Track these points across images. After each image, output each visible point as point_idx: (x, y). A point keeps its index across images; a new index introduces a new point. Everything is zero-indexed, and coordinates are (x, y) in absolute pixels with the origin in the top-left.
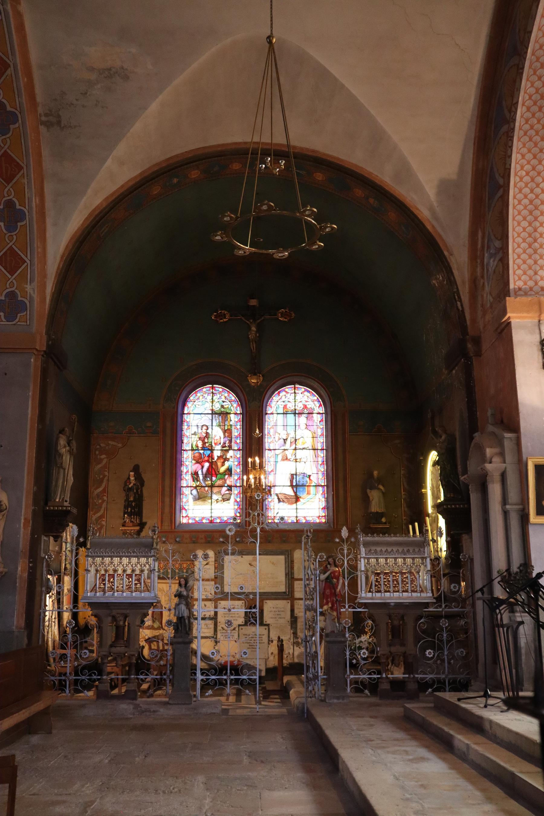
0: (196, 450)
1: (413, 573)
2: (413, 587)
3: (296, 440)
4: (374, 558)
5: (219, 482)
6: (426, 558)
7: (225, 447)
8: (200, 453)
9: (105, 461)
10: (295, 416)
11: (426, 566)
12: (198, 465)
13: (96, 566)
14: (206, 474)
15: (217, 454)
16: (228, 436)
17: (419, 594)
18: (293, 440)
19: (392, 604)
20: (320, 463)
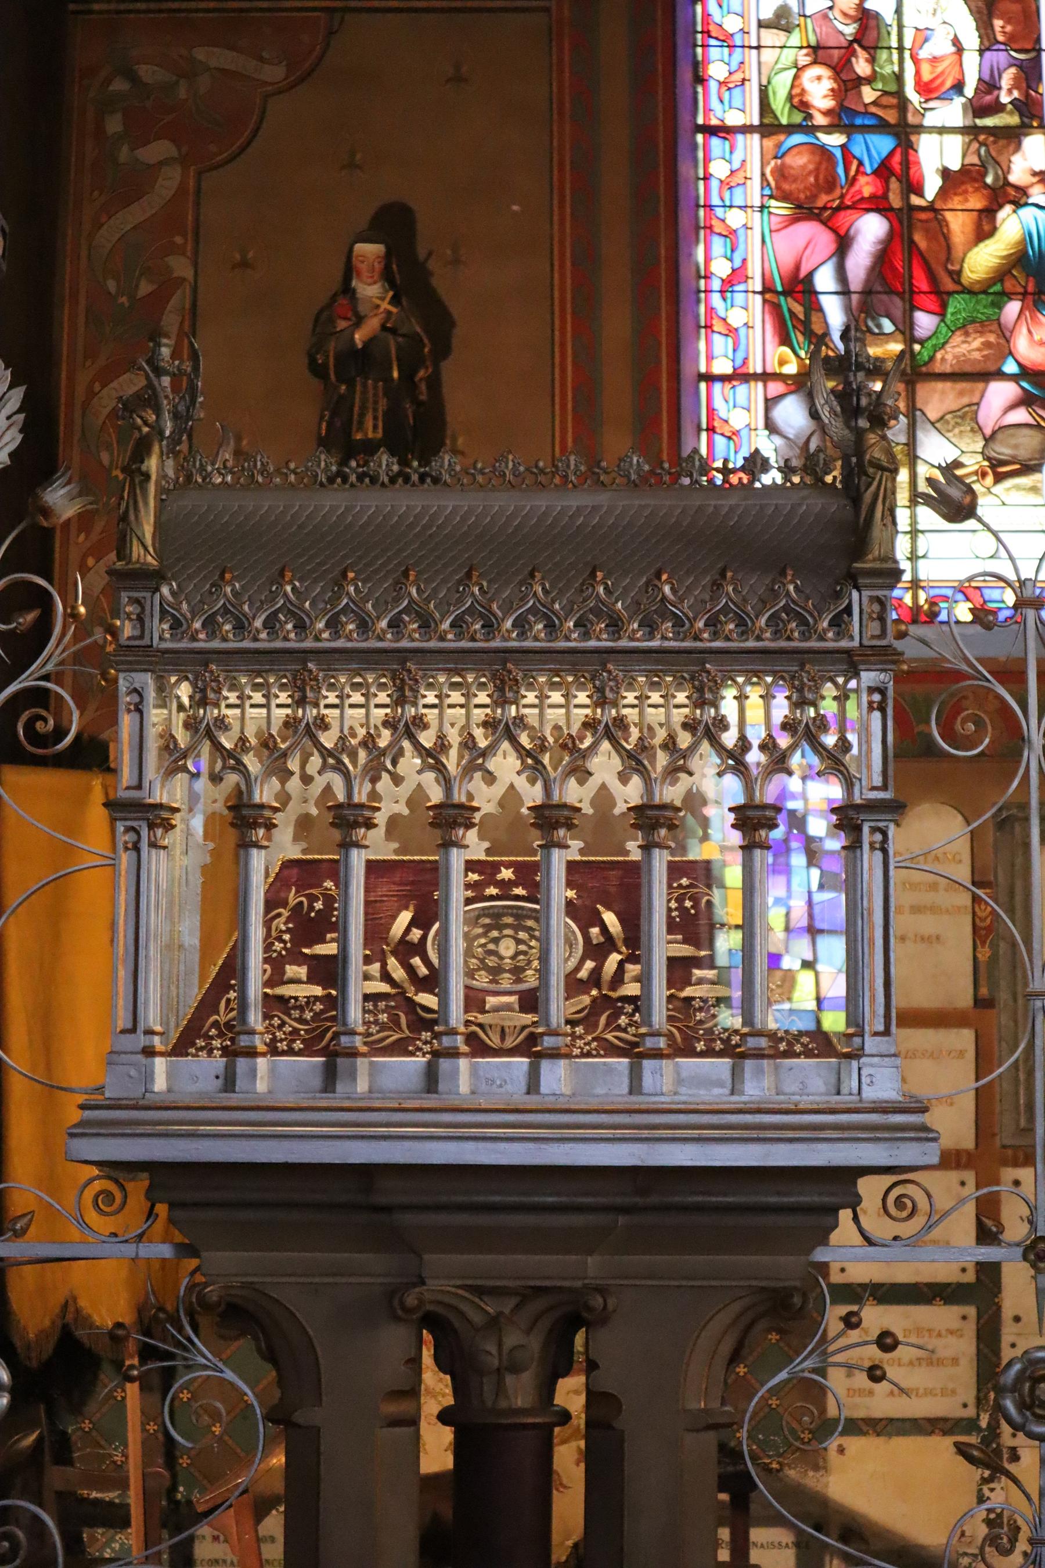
0: (791, 129)
5: (964, 349)
7: (997, 108)
8: (824, 151)
9: (168, 182)
12: (807, 230)
13: (232, 759)
14: (867, 292)
15: (938, 154)
16: (1011, 41)
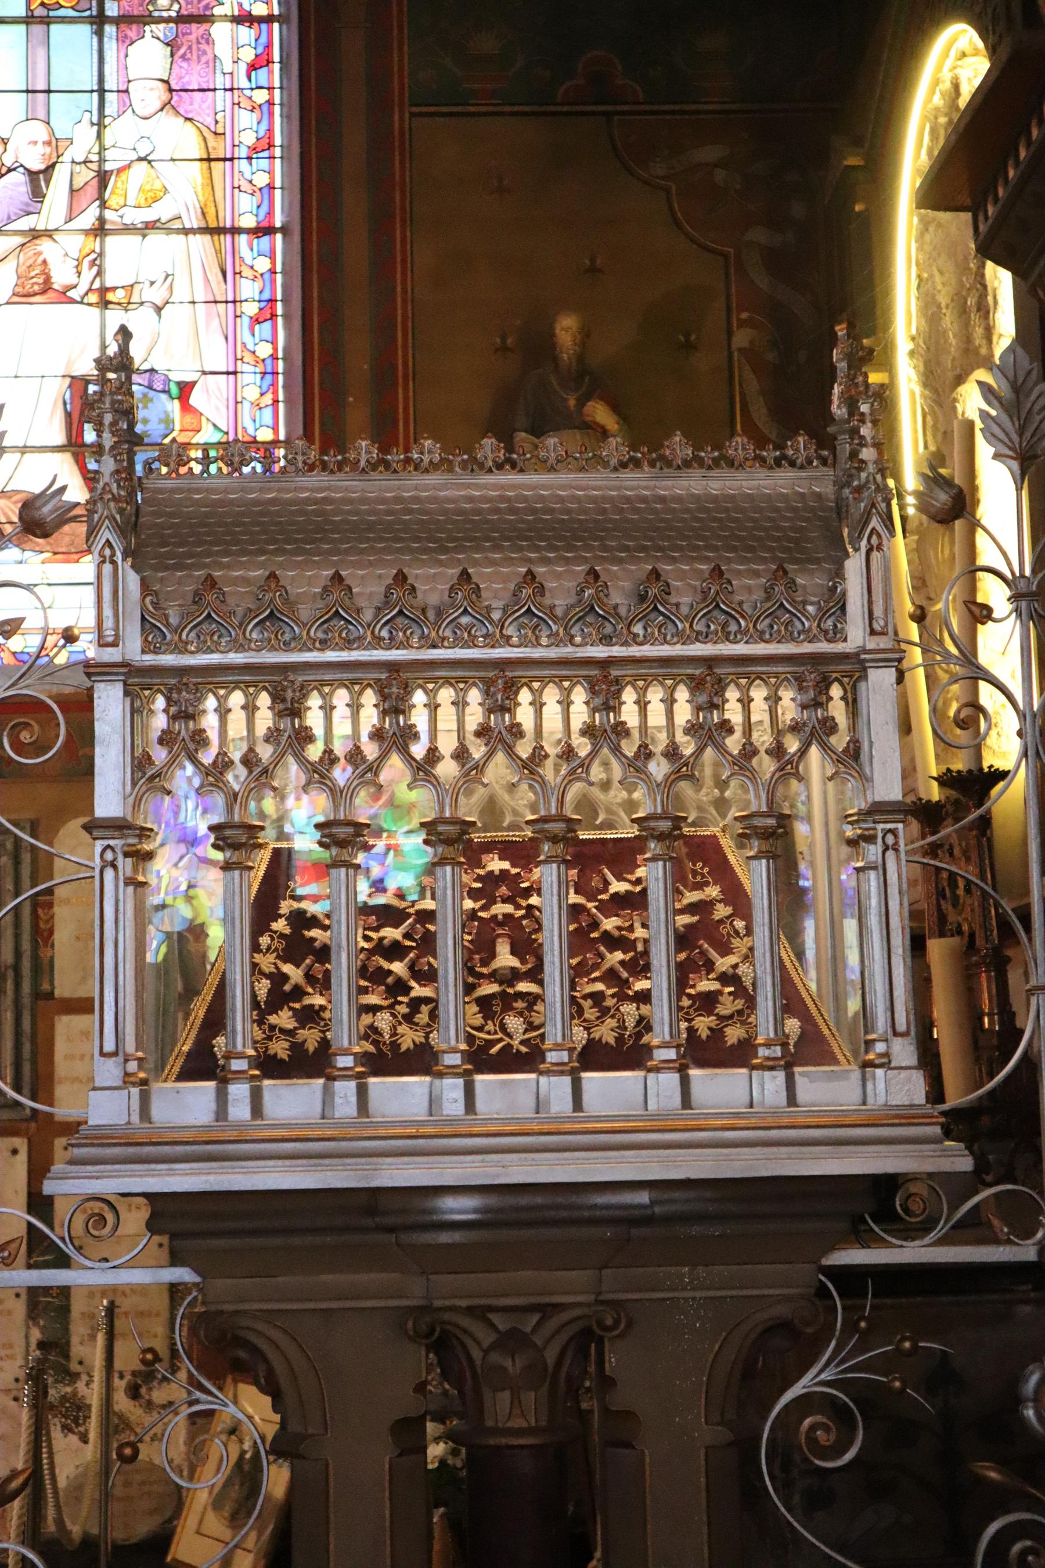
1: (707, 851)
2: (708, 1002)
3: (103, 178)
4: (249, 677)
6: (854, 669)
10: (100, 34)
11: (852, 759)
17: (770, 1087)
18: (85, 175)
19: (458, 1208)
20: (251, 309)
